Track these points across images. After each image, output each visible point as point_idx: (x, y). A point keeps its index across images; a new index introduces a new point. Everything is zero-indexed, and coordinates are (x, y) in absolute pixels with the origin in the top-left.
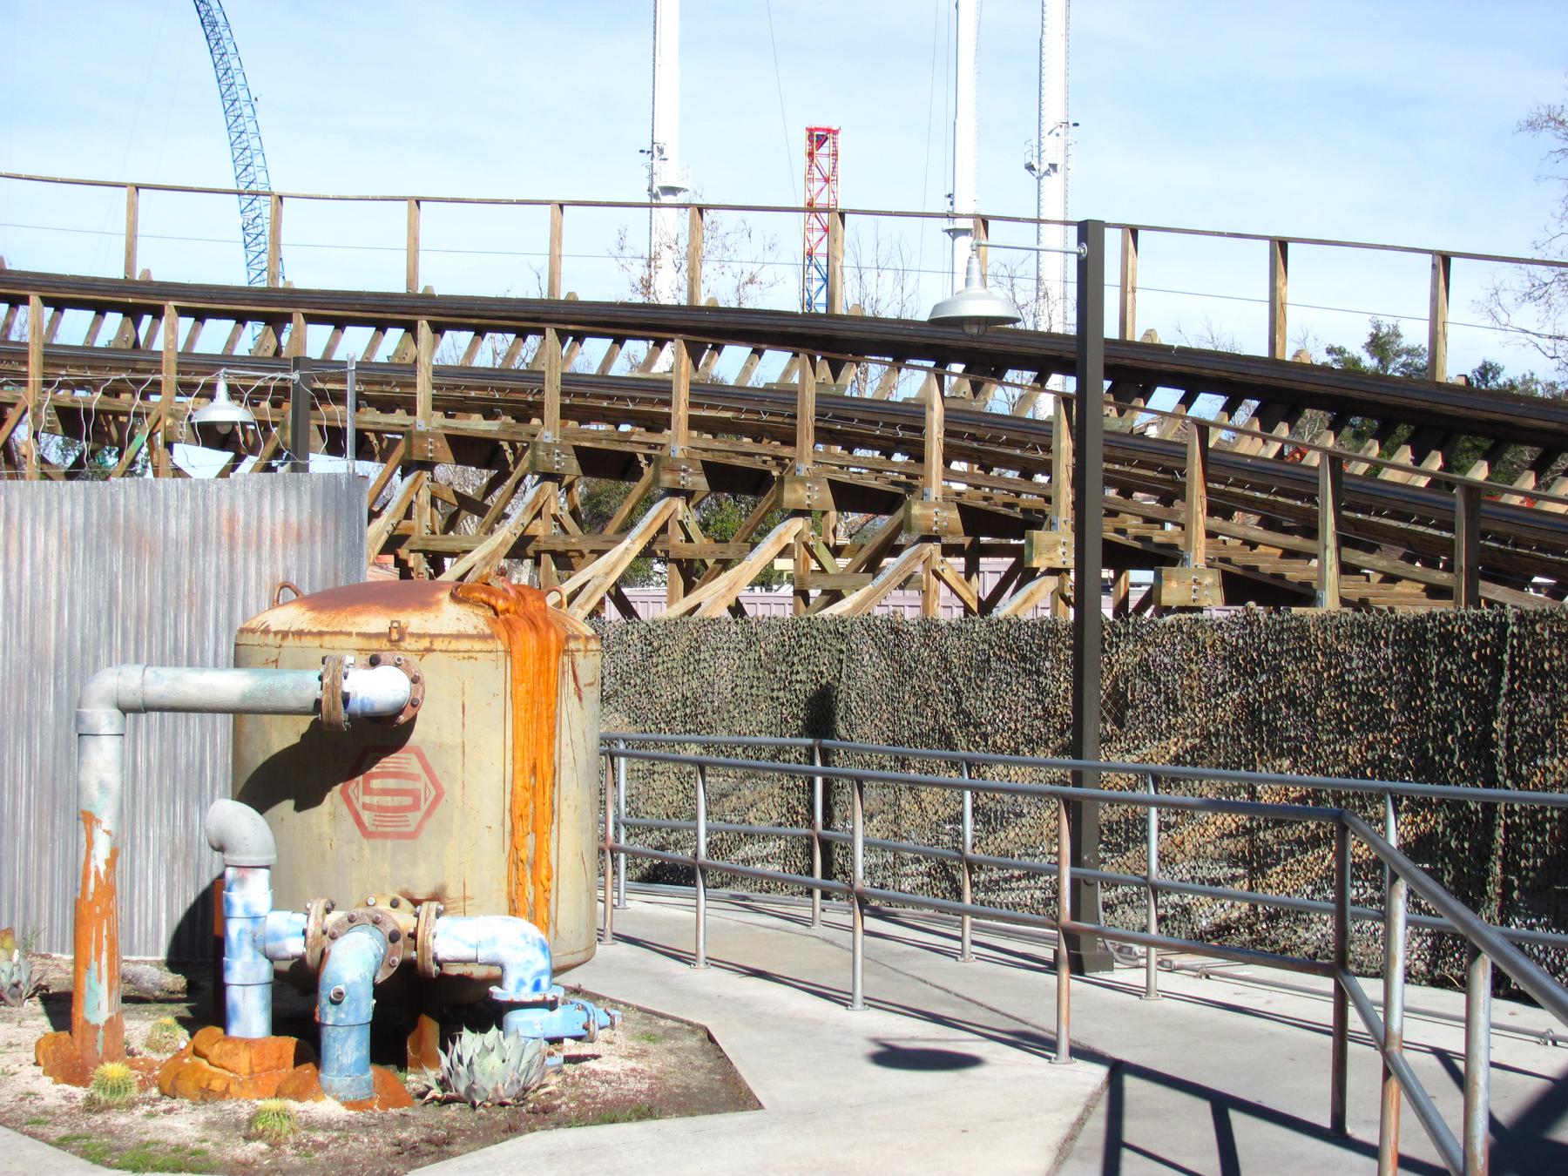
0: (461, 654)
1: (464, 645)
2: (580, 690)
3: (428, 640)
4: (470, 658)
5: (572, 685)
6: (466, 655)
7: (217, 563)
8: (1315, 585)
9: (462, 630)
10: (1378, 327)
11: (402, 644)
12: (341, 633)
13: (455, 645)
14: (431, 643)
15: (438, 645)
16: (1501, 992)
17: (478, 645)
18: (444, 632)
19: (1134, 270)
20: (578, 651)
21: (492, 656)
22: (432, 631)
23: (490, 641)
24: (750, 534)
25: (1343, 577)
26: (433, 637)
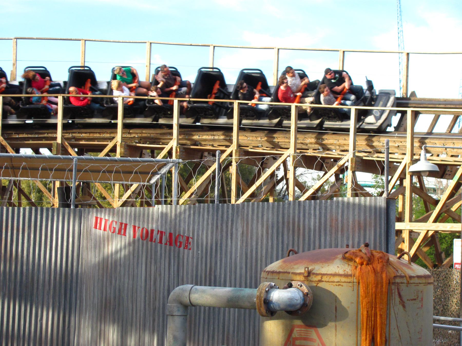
0: (335, 283)
1: (337, 279)
2: (403, 302)
3: (320, 276)
4: (339, 285)
5: (398, 299)
6: (338, 284)
7: (128, 282)
8: (300, 110)
9: (337, 272)
10: (313, 270)
11: (309, 278)
12: (286, 272)
13: (332, 279)
14: (322, 278)
15: (325, 279)
16: (191, 96)
17: (343, 279)
18: (328, 273)
19: (82, 57)
20: (402, 283)
21: (350, 284)
22: (323, 273)
23: (350, 278)
24: (379, 261)
25: (124, 129)
26: (323, 275)
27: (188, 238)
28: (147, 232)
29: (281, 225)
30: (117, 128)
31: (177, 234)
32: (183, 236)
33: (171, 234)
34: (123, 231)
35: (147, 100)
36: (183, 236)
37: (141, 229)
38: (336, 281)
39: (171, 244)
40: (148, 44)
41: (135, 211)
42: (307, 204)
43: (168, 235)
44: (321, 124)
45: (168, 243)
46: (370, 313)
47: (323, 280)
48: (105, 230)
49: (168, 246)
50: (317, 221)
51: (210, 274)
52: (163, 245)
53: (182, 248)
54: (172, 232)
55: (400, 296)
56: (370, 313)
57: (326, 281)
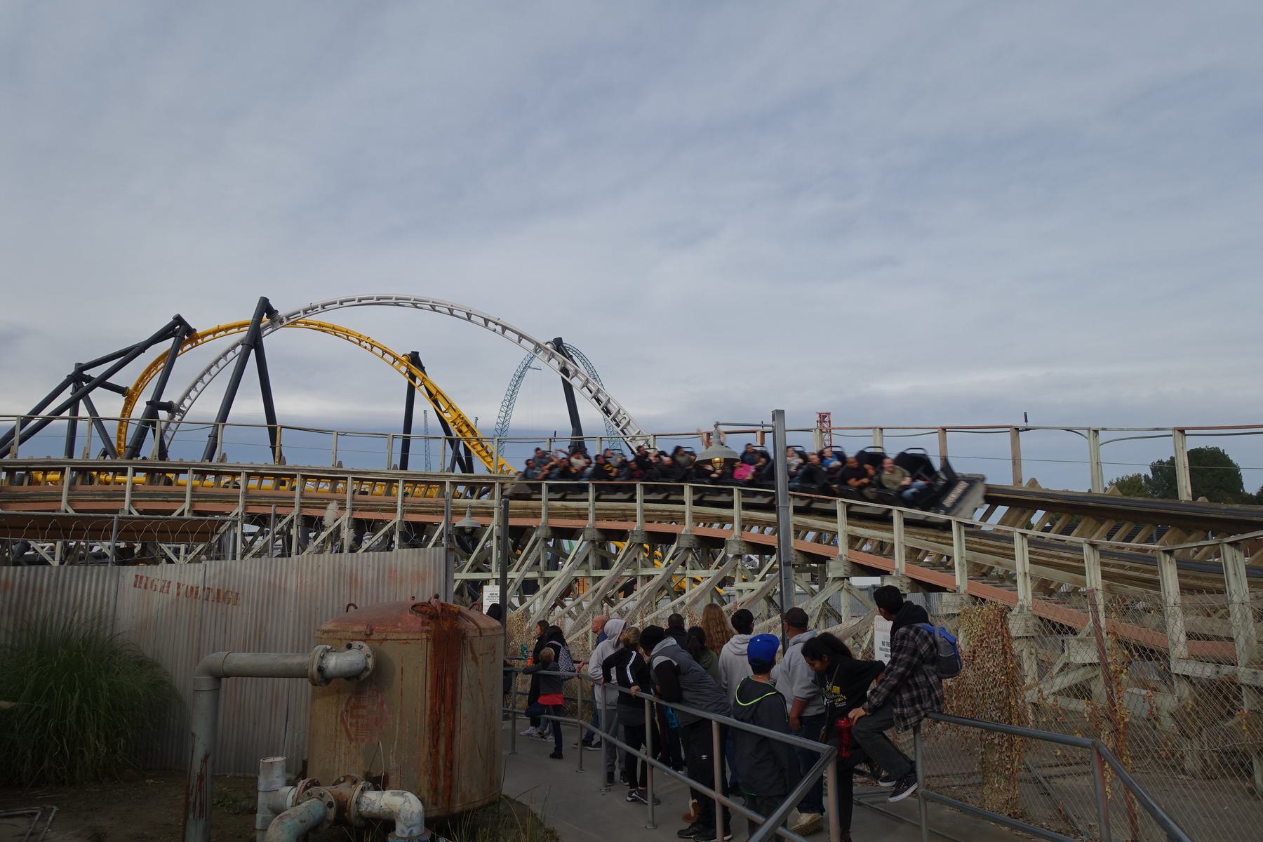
4: (407, 643)
5: (470, 656)
6: (404, 642)
27: (237, 594)
28: (192, 588)
29: (337, 575)
30: (952, 530)
31: (225, 591)
32: (232, 592)
33: (219, 591)
34: (166, 588)
35: (1008, 524)
36: (232, 592)
37: (185, 586)
38: (389, 641)
39: (218, 601)
40: (548, 441)
41: (226, 566)
42: (432, 552)
43: (216, 591)
44: (667, 496)
45: (216, 600)
46: (440, 674)
47: (388, 638)
48: (146, 588)
49: (215, 603)
50: (376, 572)
51: (260, 631)
52: (210, 602)
53: (230, 605)
54: (221, 588)
55: (473, 652)
56: (440, 674)
57: (391, 640)
